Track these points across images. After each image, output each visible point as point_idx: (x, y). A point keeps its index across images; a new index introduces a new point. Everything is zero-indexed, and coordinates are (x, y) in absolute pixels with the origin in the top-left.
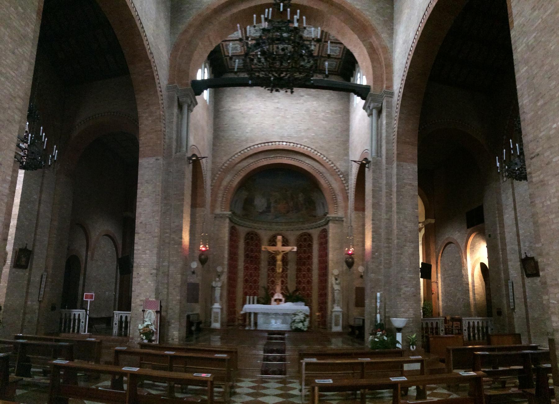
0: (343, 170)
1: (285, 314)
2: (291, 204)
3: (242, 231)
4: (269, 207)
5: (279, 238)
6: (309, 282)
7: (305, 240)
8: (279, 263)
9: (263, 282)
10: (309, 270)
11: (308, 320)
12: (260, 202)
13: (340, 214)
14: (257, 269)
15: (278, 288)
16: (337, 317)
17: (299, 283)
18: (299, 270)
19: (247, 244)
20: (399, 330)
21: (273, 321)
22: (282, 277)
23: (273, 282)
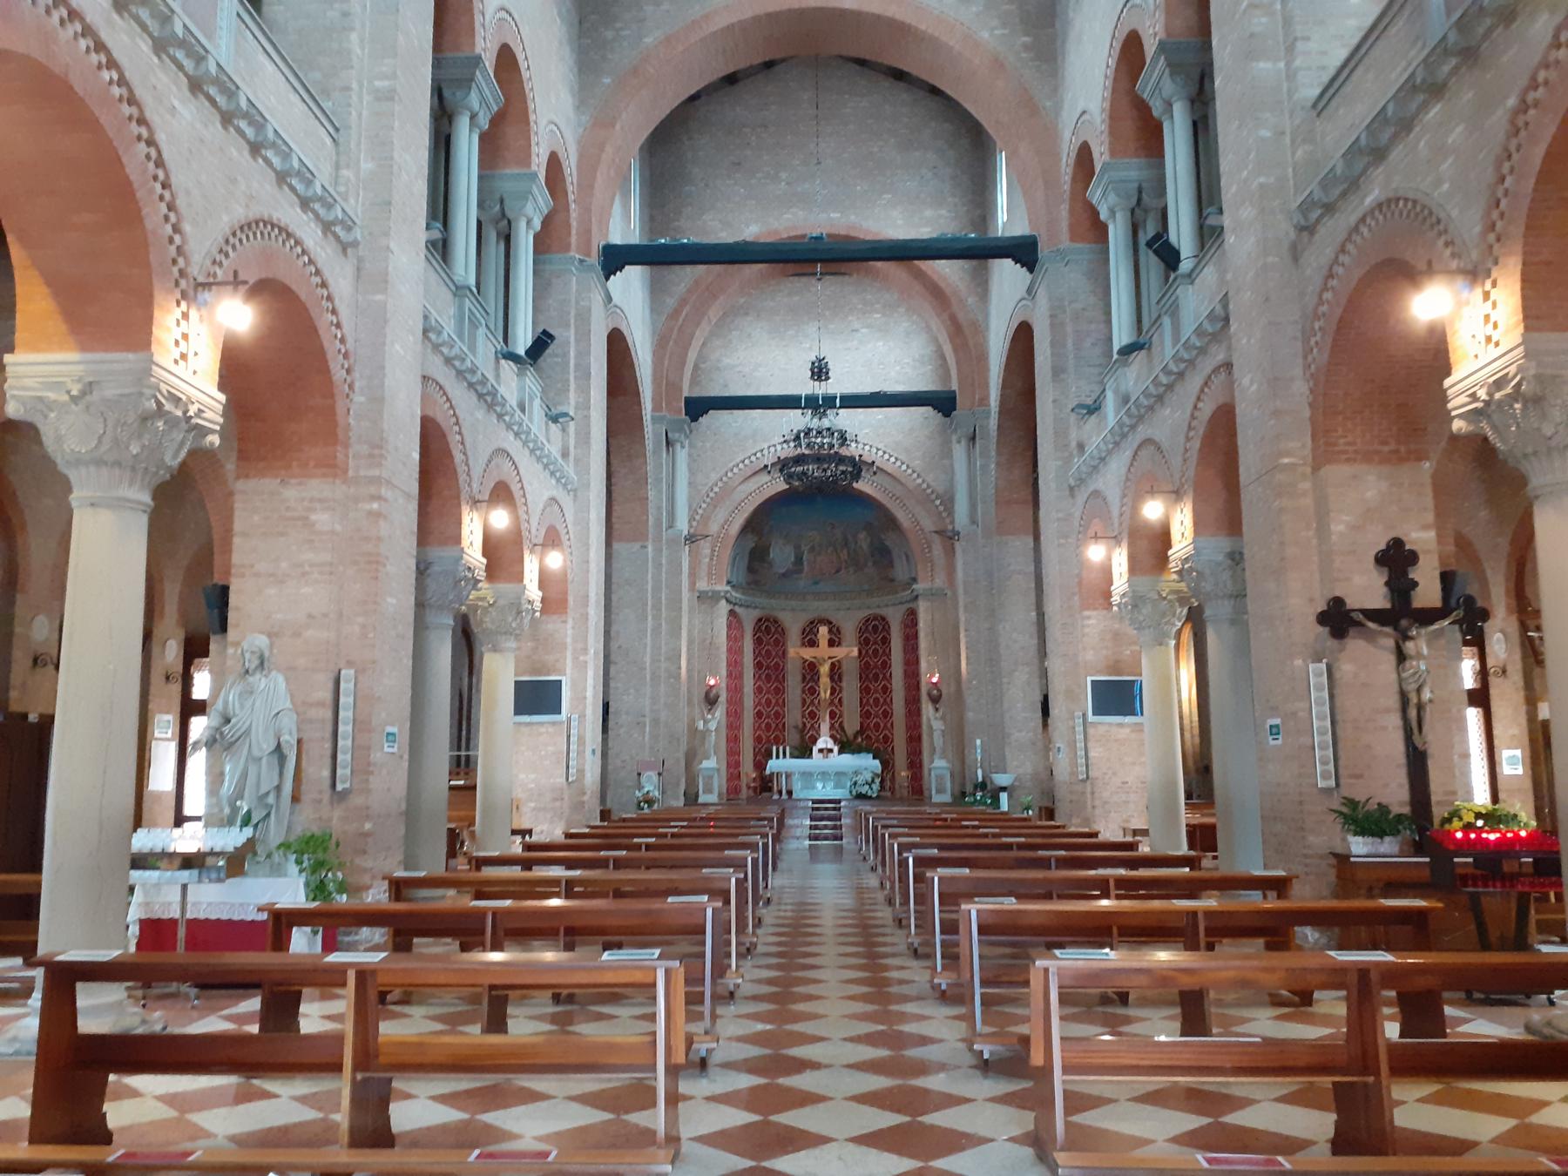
0: (940, 489)
1: (838, 774)
2: (844, 555)
3: (749, 618)
4: (799, 560)
5: (823, 630)
6: (887, 714)
7: (875, 628)
8: (825, 681)
9: (793, 716)
10: (886, 690)
11: (878, 781)
12: (781, 555)
13: (940, 581)
14: (780, 691)
15: (825, 727)
16: (940, 778)
17: (866, 715)
18: (865, 691)
19: (758, 642)
20: (1004, 789)
21: (819, 785)
22: (832, 703)
23: (813, 715)
